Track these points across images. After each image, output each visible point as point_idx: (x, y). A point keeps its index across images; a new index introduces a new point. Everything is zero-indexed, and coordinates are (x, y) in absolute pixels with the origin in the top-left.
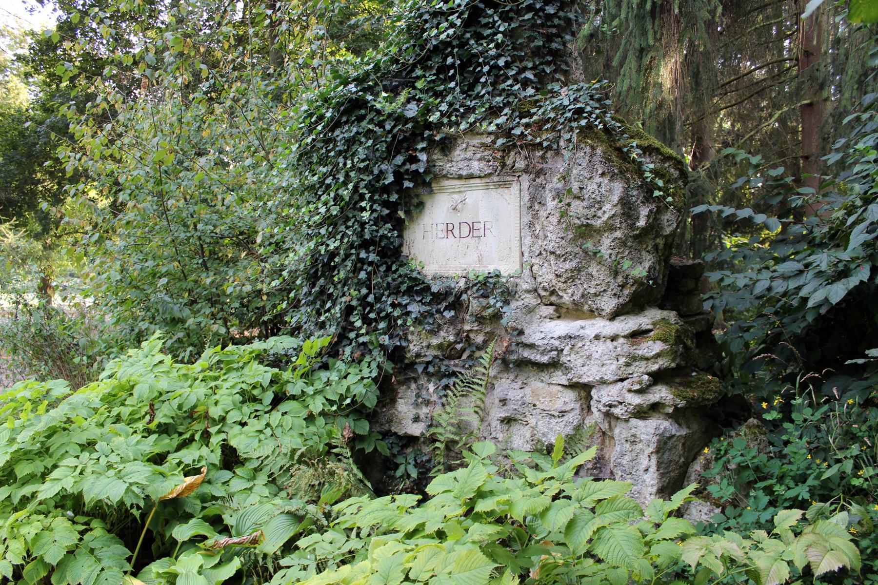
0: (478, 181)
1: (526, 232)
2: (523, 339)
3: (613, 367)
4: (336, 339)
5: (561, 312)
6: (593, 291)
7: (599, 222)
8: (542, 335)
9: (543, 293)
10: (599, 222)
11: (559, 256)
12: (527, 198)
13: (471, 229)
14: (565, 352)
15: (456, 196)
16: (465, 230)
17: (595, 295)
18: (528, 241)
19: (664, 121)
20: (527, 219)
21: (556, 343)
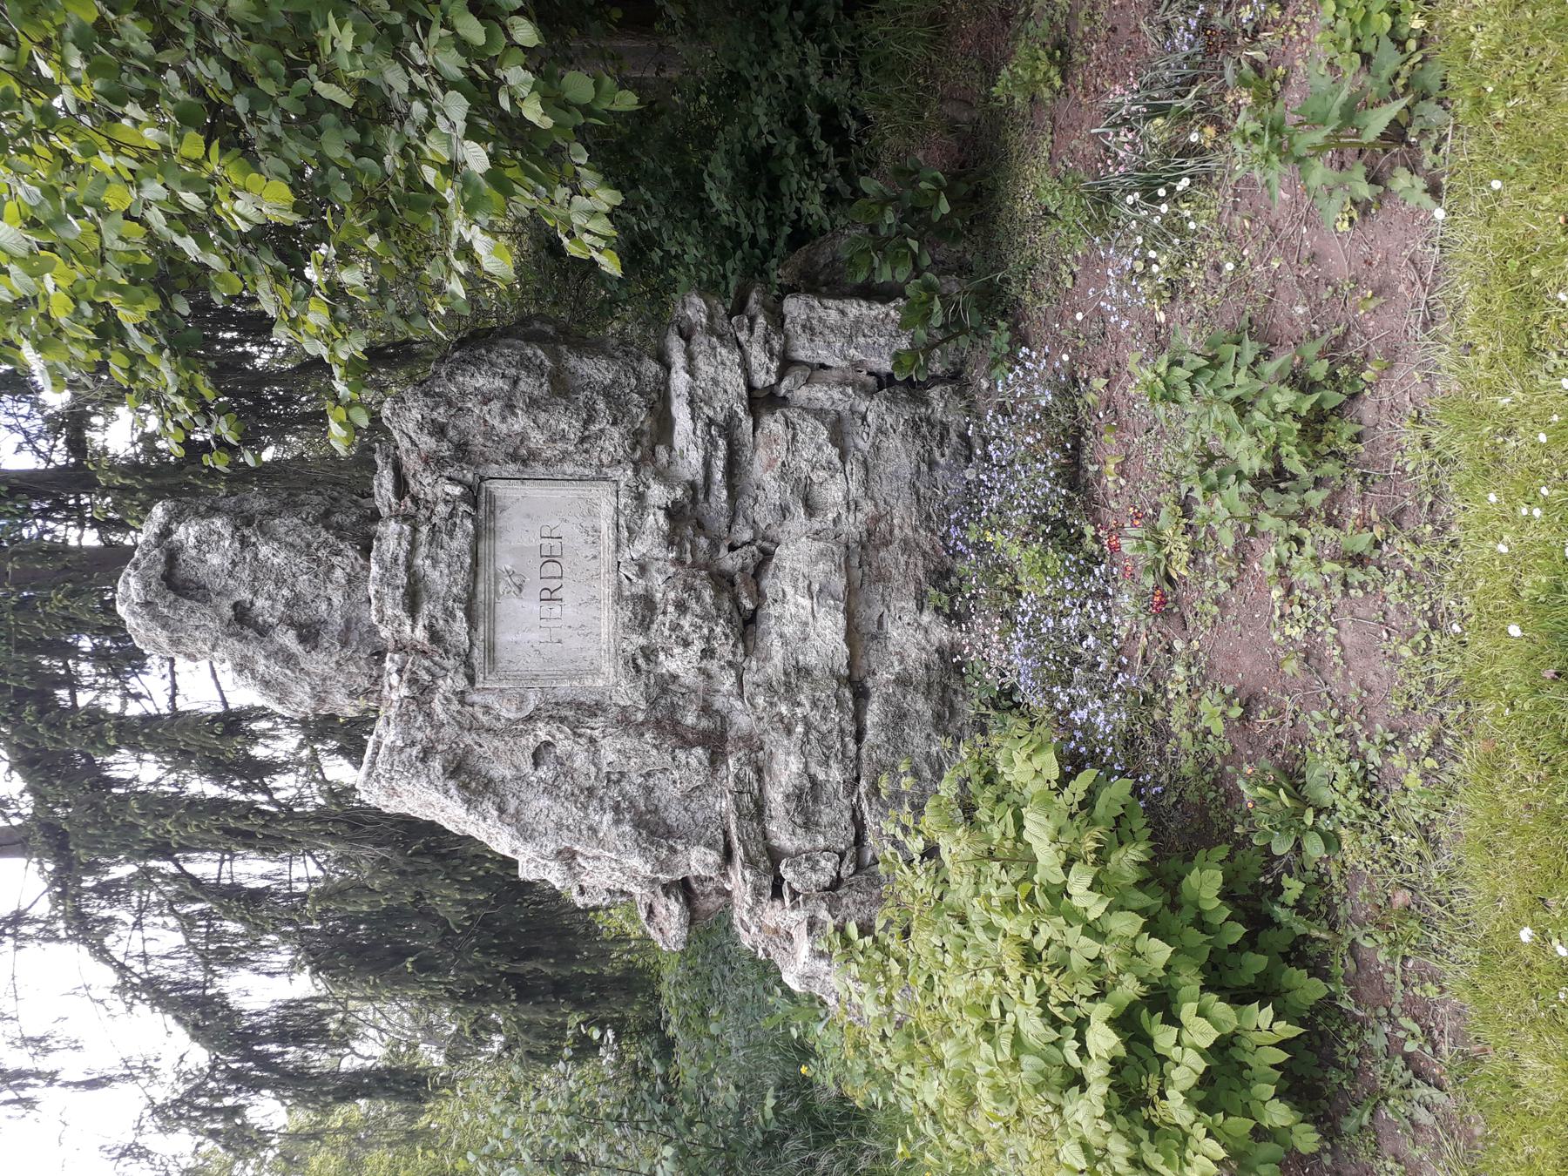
0: (481, 546)
1: (556, 471)
2: (699, 479)
3: (724, 351)
4: (505, 104)
5: (665, 425)
6: (633, 381)
7: (547, 363)
8: (692, 446)
9: (638, 454)
10: (547, 363)
11: (590, 416)
12: (512, 468)
13: (551, 559)
14: (711, 414)
15: (502, 587)
16: (552, 569)
17: (638, 379)
18: (569, 468)
19: (469, 72)
20: (540, 469)
21: (699, 425)
